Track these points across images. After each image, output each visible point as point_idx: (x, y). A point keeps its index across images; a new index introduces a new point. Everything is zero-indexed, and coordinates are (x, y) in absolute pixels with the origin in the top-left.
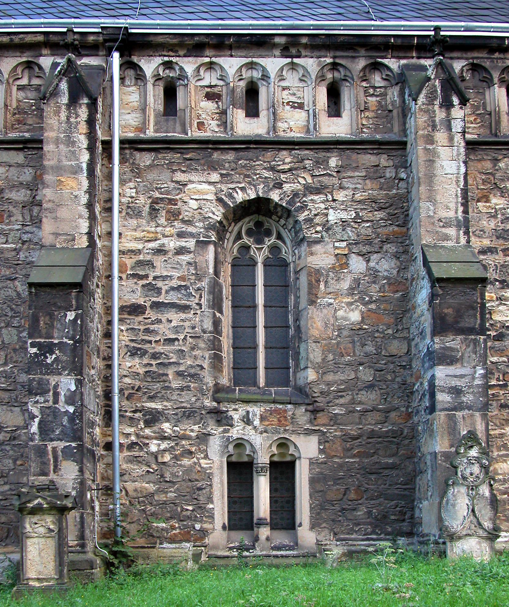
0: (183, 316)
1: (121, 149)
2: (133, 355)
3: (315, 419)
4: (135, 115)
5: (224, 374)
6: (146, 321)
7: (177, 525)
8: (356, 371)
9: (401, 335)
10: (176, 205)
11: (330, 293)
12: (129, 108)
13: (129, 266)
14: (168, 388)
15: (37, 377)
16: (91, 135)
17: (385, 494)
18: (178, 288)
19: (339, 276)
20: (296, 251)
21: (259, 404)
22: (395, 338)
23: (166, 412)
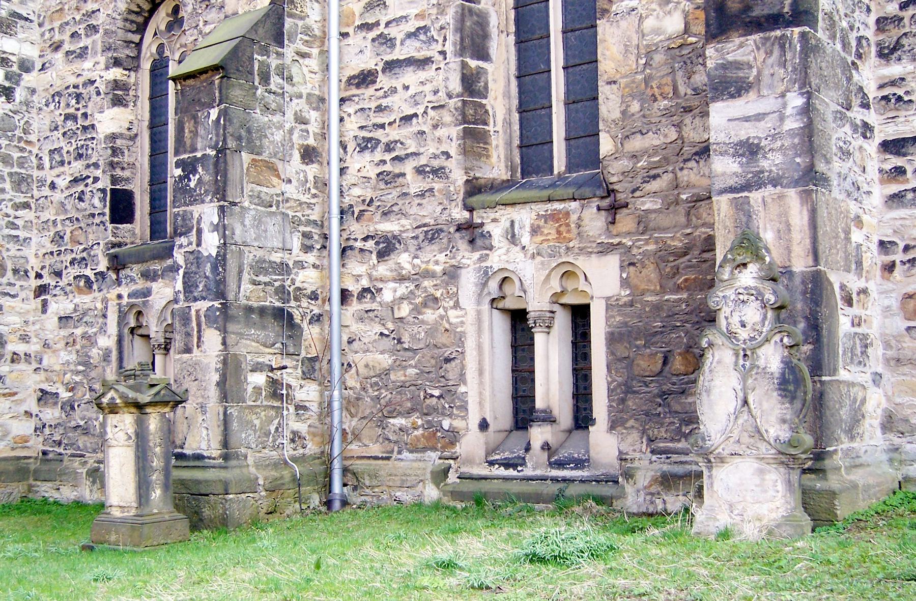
0: (422, 75)
5: (494, 159)
7: (420, 422)
8: (678, 126)
13: (357, 14)
21: (528, 206)
23: (404, 235)
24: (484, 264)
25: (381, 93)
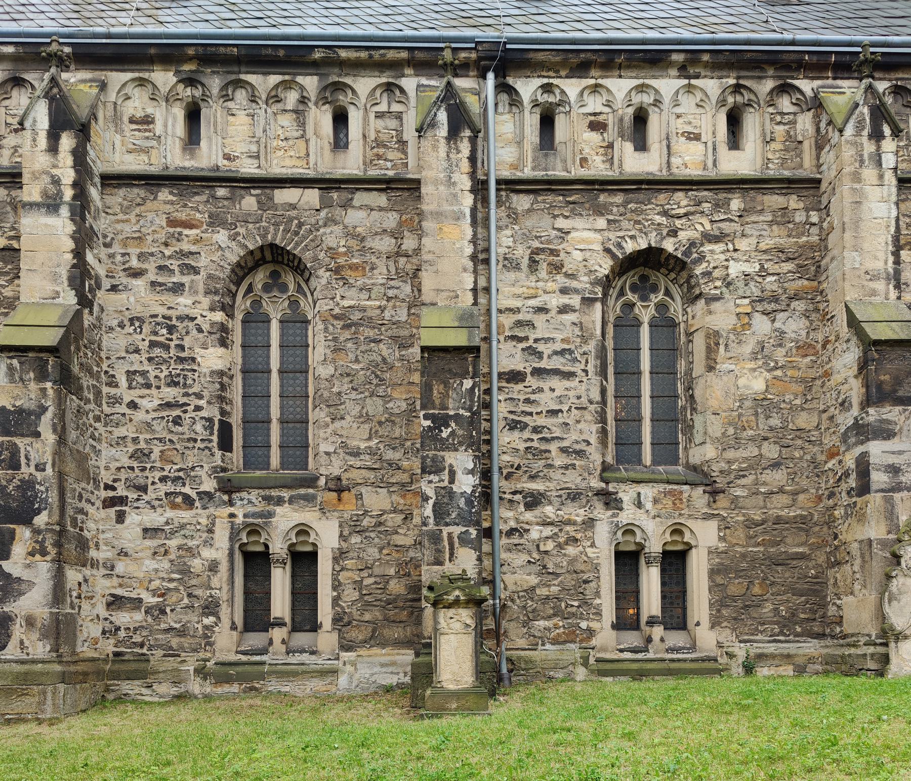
0: (567, 383)
1: (498, 190)
2: (512, 429)
3: (714, 502)
4: (509, 149)
6: (526, 390)
7: (561, 624)
8: (759, 447)
9: (811, 406)
10: (558, 256)
11: (731, 358)
12: (510, 142)
14: (550, 466)
15: (431, 454)
16: (473, 174)
17: (794, 589)
18: (562, 353)
19: (740, 338)
20: (689, 310)
21: (651, 484)
22: (803, 409)
24: (615, 519)
25: (530, 390)
